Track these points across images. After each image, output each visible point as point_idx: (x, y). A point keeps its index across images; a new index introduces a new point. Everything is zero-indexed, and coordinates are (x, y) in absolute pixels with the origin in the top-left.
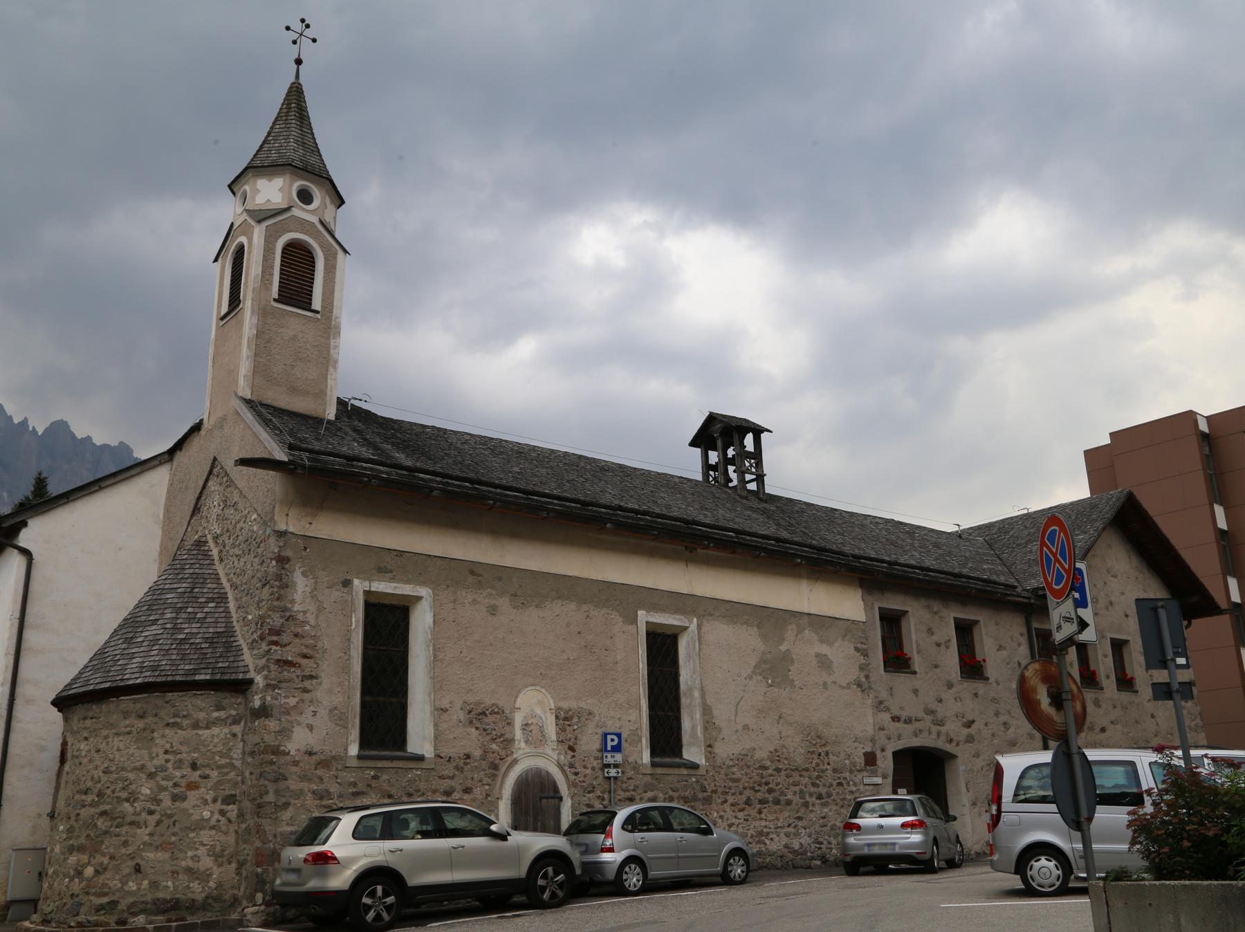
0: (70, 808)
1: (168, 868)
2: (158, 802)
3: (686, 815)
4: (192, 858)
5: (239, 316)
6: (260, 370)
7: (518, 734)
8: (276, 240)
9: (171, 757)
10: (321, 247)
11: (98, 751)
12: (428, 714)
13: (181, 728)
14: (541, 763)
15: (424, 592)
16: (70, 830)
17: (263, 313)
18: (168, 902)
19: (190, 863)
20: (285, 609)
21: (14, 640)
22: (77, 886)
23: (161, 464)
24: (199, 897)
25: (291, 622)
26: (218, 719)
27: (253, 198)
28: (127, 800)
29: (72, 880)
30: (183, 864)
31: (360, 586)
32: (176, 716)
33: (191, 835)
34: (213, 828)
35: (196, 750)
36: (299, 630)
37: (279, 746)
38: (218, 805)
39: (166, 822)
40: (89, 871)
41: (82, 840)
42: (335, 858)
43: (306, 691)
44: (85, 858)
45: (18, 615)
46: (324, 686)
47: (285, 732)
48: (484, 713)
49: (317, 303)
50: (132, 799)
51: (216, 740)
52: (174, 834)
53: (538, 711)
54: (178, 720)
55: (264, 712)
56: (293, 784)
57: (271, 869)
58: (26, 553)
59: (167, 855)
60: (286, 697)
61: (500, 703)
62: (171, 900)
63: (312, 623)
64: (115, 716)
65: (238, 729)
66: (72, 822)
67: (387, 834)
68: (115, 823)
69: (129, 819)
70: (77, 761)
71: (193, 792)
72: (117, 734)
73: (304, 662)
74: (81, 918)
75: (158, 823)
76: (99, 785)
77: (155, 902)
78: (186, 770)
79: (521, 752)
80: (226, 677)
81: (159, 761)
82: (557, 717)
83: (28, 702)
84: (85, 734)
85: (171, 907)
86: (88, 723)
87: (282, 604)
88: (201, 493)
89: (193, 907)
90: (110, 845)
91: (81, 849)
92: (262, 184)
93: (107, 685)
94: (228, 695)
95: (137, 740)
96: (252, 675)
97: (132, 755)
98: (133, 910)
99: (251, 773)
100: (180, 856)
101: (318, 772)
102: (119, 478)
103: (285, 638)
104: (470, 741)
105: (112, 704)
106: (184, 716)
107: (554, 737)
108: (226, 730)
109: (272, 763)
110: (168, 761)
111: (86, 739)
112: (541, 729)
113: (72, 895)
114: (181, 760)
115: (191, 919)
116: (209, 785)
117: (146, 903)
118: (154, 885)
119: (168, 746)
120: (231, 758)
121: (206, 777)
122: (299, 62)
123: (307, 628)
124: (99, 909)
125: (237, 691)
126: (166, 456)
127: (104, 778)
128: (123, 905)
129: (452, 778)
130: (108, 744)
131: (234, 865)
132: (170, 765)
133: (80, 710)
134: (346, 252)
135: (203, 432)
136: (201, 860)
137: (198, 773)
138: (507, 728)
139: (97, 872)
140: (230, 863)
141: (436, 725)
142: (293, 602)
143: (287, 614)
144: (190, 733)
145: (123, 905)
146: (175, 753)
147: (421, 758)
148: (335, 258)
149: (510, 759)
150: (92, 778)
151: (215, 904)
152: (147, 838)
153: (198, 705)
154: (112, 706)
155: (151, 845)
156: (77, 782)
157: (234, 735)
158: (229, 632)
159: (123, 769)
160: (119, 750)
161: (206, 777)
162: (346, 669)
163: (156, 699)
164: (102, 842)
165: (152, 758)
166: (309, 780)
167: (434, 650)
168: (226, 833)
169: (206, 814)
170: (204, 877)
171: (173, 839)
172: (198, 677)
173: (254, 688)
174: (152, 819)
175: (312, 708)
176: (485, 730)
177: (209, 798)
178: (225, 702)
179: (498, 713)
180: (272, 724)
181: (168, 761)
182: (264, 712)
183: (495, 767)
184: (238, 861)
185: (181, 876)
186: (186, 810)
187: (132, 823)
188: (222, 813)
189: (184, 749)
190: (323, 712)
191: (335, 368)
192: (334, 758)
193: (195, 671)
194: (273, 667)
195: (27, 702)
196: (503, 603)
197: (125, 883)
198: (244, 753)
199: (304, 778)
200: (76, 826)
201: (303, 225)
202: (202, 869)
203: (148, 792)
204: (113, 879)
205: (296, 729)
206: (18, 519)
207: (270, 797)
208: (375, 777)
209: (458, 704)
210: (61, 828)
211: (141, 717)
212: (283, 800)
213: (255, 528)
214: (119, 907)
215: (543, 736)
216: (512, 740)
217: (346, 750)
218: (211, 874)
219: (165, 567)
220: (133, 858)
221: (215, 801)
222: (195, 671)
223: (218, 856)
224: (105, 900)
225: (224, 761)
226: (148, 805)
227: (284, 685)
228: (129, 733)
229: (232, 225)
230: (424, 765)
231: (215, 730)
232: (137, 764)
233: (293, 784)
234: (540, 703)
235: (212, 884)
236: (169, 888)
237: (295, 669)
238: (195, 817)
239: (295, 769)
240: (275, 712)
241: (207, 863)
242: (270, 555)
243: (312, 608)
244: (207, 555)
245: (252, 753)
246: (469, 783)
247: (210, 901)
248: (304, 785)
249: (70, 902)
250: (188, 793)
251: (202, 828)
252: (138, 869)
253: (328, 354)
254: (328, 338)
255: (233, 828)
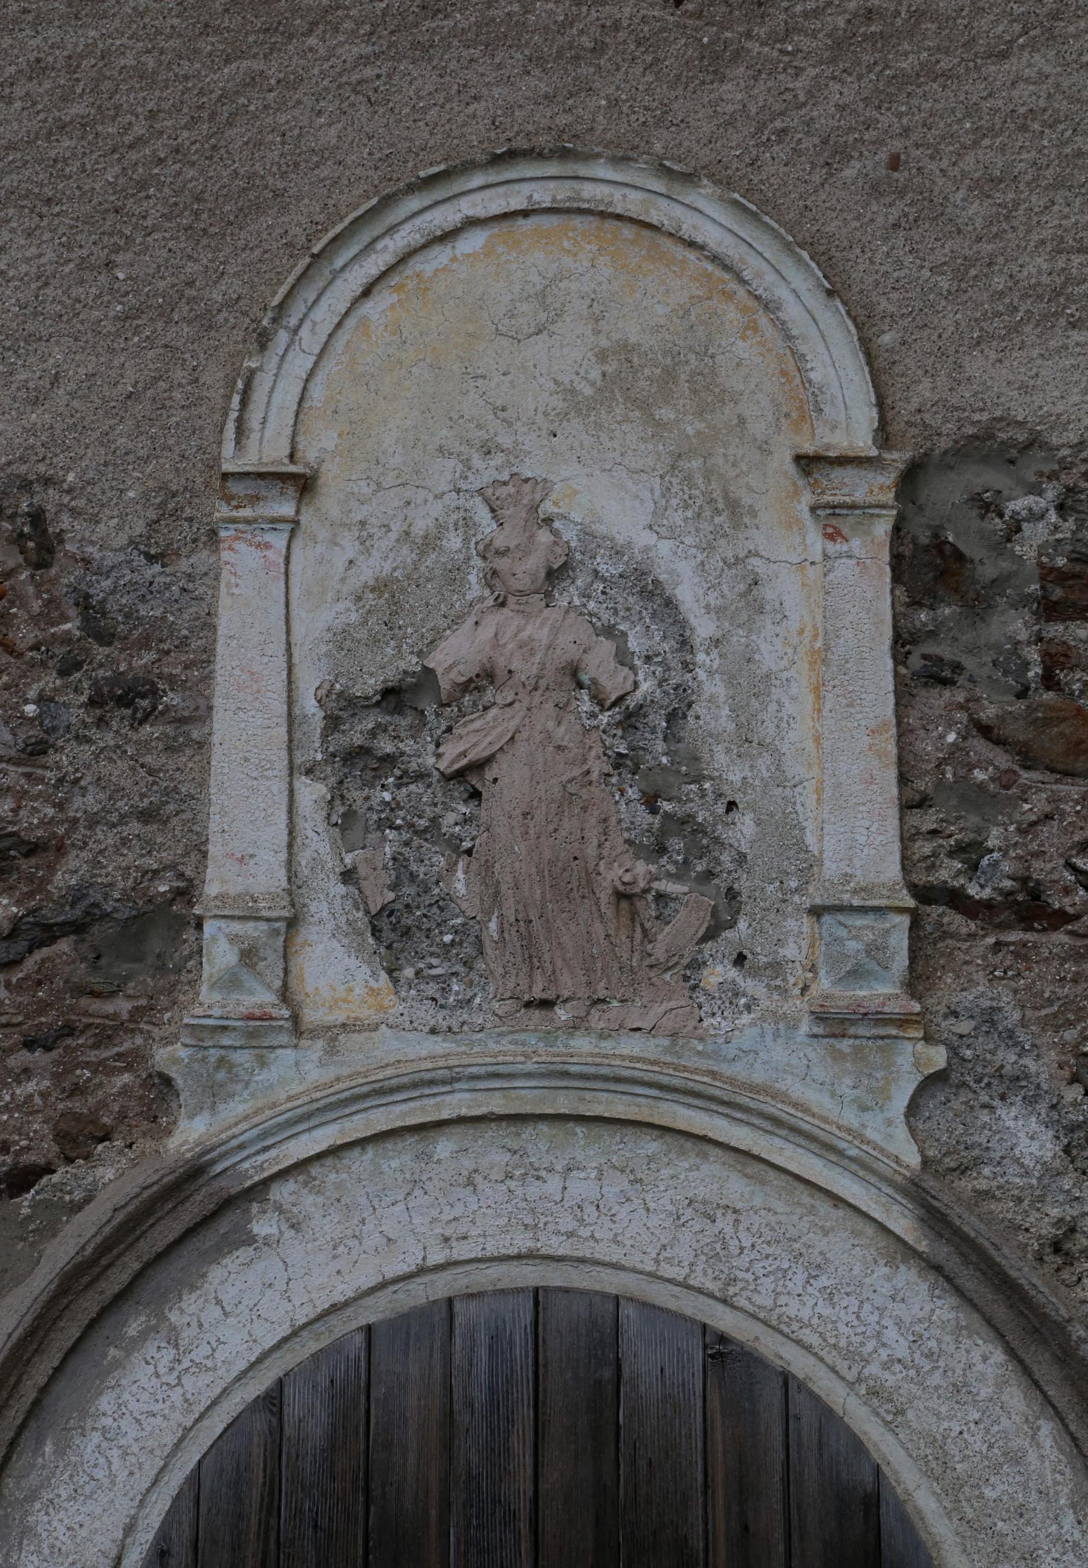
3: (368, 308)
7: (254, 816)
14: (625, 1226)
53: (611, 501)
79: (295, 1072)
82: (927, 570)
107: (858, 838)
112: (647, 745)
138: (102, 764)
149: (113, 1179)
215: (682, 836)
216: (156, 925)
234: (638, 385)
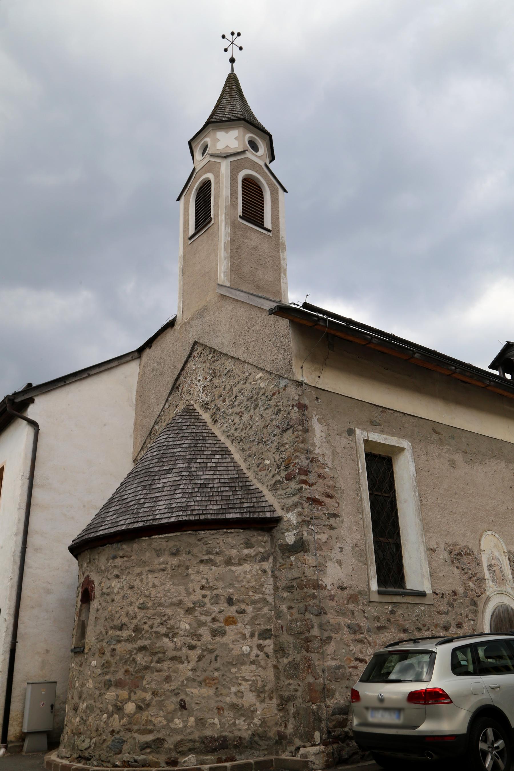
0: (104, 644)
1: (213, 704)
2: (199, 637)
4: (236, 694)
5: (211, 231)
6: (235, 269)
7: (487, 575)
8: (238, 173)
9: (208, 593)
10: (268, 184)
11: (132, 588)
12: (423, 554)
13: (215, 565)
15: (405, 444)
16: (106, 666)
17: (233, 226)
18: (216, 740)
19: (234, 699)
20: (308, 452)
21: (25, 497)
22: (116, 722)
23: (132, 360)
24: (246, 735)
25: (314, 464)
26: (248, 556)
27: (215, 145)
28: (167, 635)
29: (110, 716)
30: (228, 700)
31: (360, 434)
32: (209, 553)
33: (234, 670)
34: (253, 663)
35: (231, 585)
36: (321, 471)
37: (318, 580)
38: (256, 640)
39: (208, 657)
40: (130, 707)
41: (120, 675)
42: (446, 696)
43: (332, 528)
44: (124, 694)
45: (28, 475)
46: (346, 524)
47: (320, 567)
48: (459, 554)
49: (268, 223)
50: (171, 634)
51: (248, 576)
52: (217, 670)
53: (496, 554)
54: (212, 557)
55: (300, 546)
56: (332, 618)
57: (323, 705)
58: (33, 424)
59: (211, 691)
60: (318, 533)
61: (470, 546)
62: (219, 738)
63: (330, 465)
64: (148, 554)
65: (267, 565)
66: (107, 656)
67: (481, 669)
68: (156, 658)
69: (170, 654)
70: (108, 598)
71: (232, 627)
72: (152, 571)
73: (327, 501)
74: (126, 757)
75: (200, 658)
76: (135, 621)
77: (203, 740)
78: (224, 606)
79: (491, 590)
80: (256, 515)
81: (197, 596)
83: (37, 550)
84: (116, 572)
85: (219, 746)
86: (119, 561)
87: (306, 446)
88: (180, 374)
89: (240, 745)
90: (151, 681)
91: (119, 684)
92: (221, 135)
93: (140, 524)
94: (255, 533)
95: (172, 577)
96: (279, 513)
97: (169, 591)
98: (183, 748)
99: (290, 608)
100: (225, 691)
101: (349, 606)
102: (102, 369)
103: (312, 478)
104: (453, 580)
105: (145, 542)
106: (217, 553)
108: (257, 567)
109: (314, 597)
110: (204, 596)
111: (117, 576)
113: (112, 732)
114: (217, 596)
115: (241, 760)
116: (246, 620)
117: (194, 741)
118: (201, 722)
119: (204, 582)
120: (263, 593)
121: (242, 612)
122: (232, 60)
123: (327, 470)
124: (145, 746)
125: (263, 530)
126: (136, 354)
127: (141, 614)
128: (169, 744)
129: (447, 613)
130: (141, 581)
131: (275, 702)
132: (207, 600)
133: (87, 555)
134: (285, 191)
135: (177, 327)
136: (243, 695)
137: (235, 608)
139: (139, 708)
140: (271, 699)
141: (430, 563)
142: (314, 445)
143: (311, 456)
144: (223, 569)
145: (169, 744)
146: (211, 588)
147: (423, 594)
148: (277, 194)
150: (127, 614)
151: (261, 743)
152: (190, 674)
153: (230, 542)
154: (144, 545)
155: (194, 680)
156: (111, 618)
157: (264, 571)
158: (242, 478)
159: (160, 605)
160: (154, 586)
161: (242, 612)
162: (360, 510)
163: (187, 538)
164: (143, 678)
165: (189, 594)
166: (344, 614)
167: (420, 497)
168: (265, 668)
169: (246, 649)
170: (248, 713)
171: (216, 674)
172: (228, 516)
173: (283, 525)
174: (194, 655)
175: (339, 545)
176: (463, 569)
177: (247, 633)
178: (254, 539)
179: (469, 554)
180: (310, 559)
181: (204, 596)
182: (300, 546)
183: (475, 603)
184: (281, 697)
185: (226, 713)
186: (227, 645)
187: (173, 659)
188: (260, 647)
189: (220, 584)
190: (347, 549)
191: (285, 274)
192: (360, 593)
193: (224, 511)
194: (306, 504)
195: (36, 550)
196: (458, 457)
197: (170, 720)
198: (276, 588)
199: (340, 612)
200: (113, 661)
201: (254, 166)
202: (246, 705)
203: (187, 627)
204: (157, 715)
205: (329, 564)
206: (27, 396)
207: (315, 632)
208: (392, 612)
209: (442, 546)
210: (94, 663)
211: (175, 554)
212: (326, 634)
213: (262, 385)
214: (166, 746)
215: (503, 575)
217: (368, 585)
218: (254, 712)
219: (140, 441)
220: (177, 694)
221: (252, 635)
222: (224, 511)
223: (259, 692)
224: (150, 738)
225: (258, 597)
226: (189, 640)
227: (315, 522)
228: (163, 570)
229: (194, 169)
230: (426, 601)
231: (247, 567)
232: (175, 600)
233: (332, 618)
234: (496, 546)
235: (256, 721)
236: (216, 726)
237: (319, 506)
238: (236, 652)
239: (331, 603)
240: (312, 547)
241: (250, 699)
242: (291, 403)
243: (328, 452)
244: (198, 418)
245: (289, 588)
246: (459, 619)
247: (256, 738)
248: (340, 619)
249: (110, 740)
250: (227, 628)
251: (243, 663)
252: (183, 706)
253: (280, 263)
254: (278, 251)
255: (272, 662)
